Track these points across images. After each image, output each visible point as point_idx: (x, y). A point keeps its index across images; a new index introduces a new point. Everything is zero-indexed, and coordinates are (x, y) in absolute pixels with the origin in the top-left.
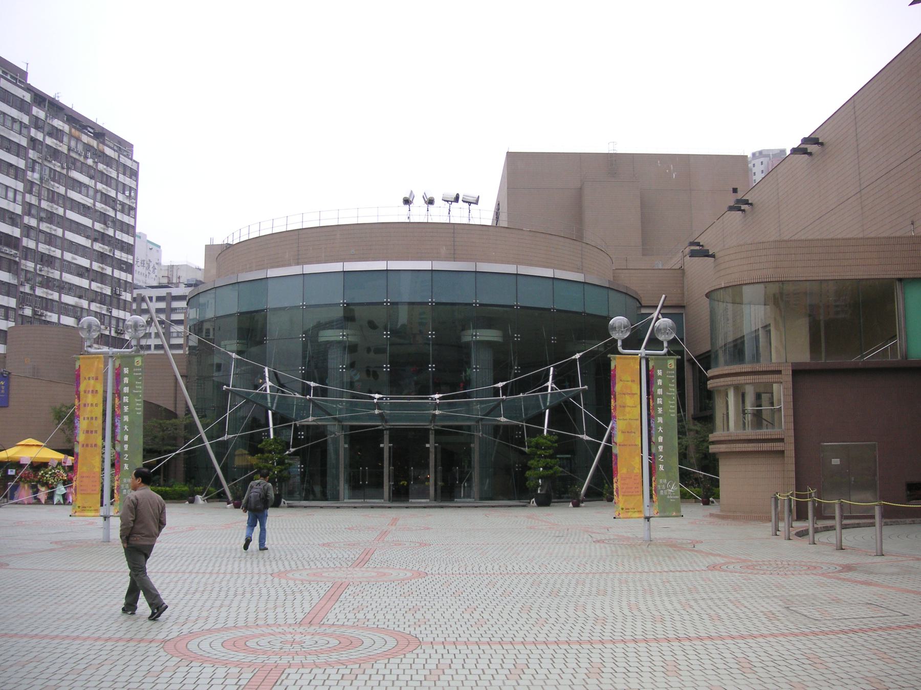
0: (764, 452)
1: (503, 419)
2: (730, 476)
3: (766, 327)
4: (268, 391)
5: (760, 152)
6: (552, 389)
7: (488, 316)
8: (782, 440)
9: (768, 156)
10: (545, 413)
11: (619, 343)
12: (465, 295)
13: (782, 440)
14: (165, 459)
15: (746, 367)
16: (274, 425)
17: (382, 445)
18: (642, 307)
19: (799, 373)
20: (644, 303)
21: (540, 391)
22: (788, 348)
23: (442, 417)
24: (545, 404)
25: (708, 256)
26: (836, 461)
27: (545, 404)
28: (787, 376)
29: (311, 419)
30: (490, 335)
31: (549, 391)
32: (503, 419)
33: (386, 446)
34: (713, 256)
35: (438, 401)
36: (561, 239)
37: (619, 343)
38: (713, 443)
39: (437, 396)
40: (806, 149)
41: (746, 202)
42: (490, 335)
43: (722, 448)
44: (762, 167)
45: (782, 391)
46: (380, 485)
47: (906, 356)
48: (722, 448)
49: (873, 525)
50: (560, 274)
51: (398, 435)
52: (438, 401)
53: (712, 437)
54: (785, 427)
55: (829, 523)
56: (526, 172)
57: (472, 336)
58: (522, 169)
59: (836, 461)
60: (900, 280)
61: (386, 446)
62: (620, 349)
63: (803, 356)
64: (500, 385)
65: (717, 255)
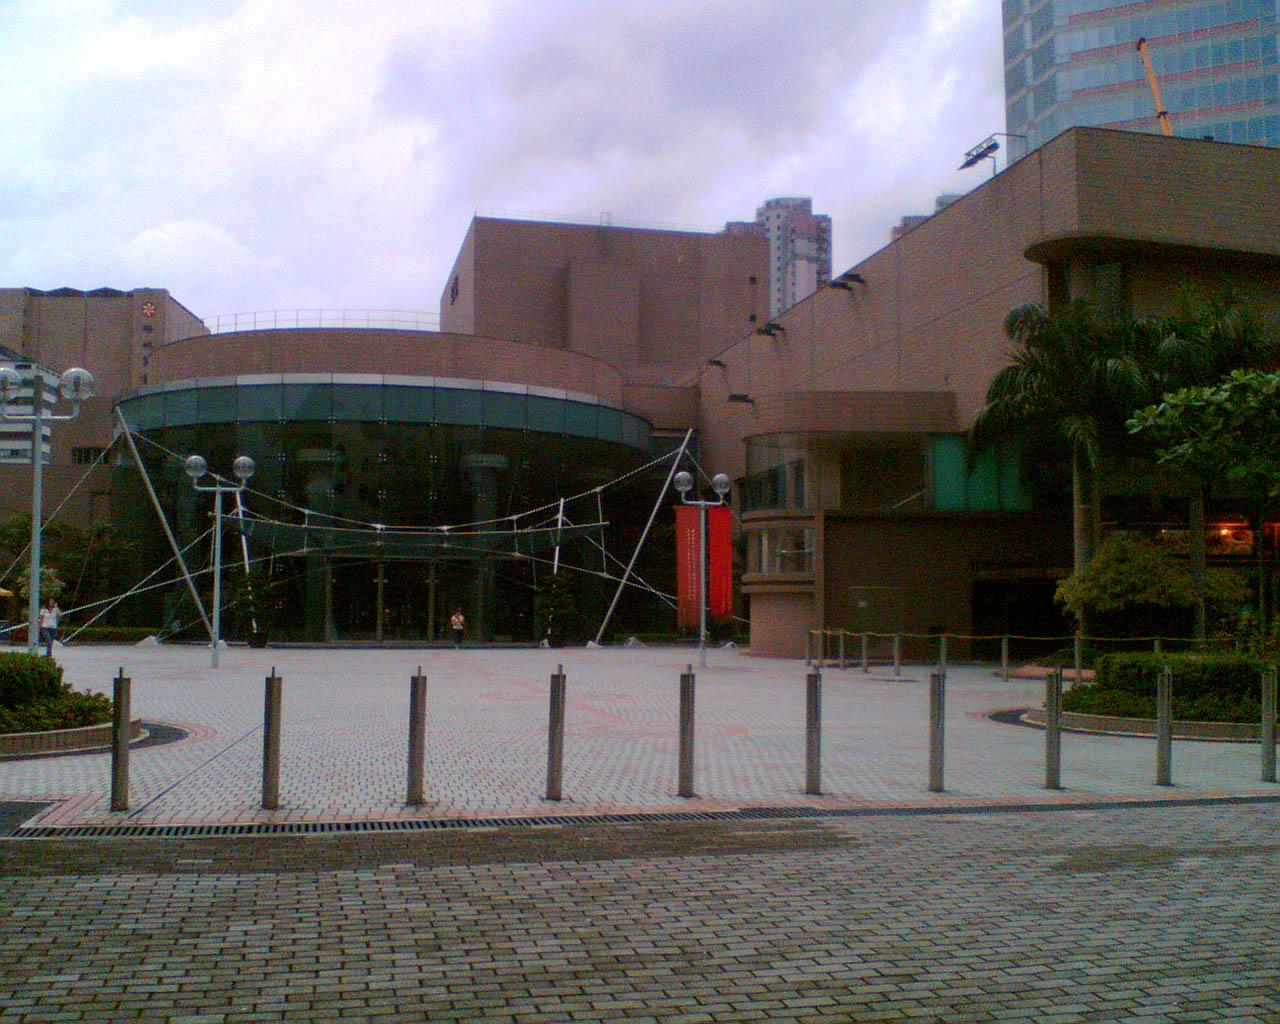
0: (793, 593)
1: (517, 554)
2: (761, 621)
3: (798, 467)
4: (241, 516)
6: (563, 525)
7: (493, 439)
8: (811, 583)
10: (555, 550)
11: (683, 495)
12: (471, 416)
13: (811, 583)
14: (139, 588)
15: (780, 512)
16: (249, 558)
17: (375, 581)
18: (654, 429)
19: (832, 521)
20: (656, 425)
21: (547, 526)
22: (822, 491)
23: (453, 551)
24: (555, 540)
25: (747, 401)
26: (862, 604)
27: (555, 540)
28: (819, 523)
29: (305, 550)
30: (497, 461)
32: (517, 554)
33: (381, 581)
34: (751, 401)
35: (447, 533)
36: (1195, 808)
37: (683, 495)
38: (745, 584)
39: (445, 528)
40: (846, 284)
41: (777, 327)
42: (497, 461)
43: (756, 589)
45: (814, 538)
46: (425, 629)
47: (931, 507)
48: (756, 589)
49: (893, 664)
50: (573, 396)
51: (393, 569)
52: (447, 533)
53: (745, 578)
54: (816, 569)
55: (836, 662)
56: (499, 252)
57: (477, 462)
58: (493, 243)
59: (862, 604)
60: (933, 435)
61: (381, 581)
62: (683, 500)
63: (836, 504)
64: (514, 517)
65: (756, 402)
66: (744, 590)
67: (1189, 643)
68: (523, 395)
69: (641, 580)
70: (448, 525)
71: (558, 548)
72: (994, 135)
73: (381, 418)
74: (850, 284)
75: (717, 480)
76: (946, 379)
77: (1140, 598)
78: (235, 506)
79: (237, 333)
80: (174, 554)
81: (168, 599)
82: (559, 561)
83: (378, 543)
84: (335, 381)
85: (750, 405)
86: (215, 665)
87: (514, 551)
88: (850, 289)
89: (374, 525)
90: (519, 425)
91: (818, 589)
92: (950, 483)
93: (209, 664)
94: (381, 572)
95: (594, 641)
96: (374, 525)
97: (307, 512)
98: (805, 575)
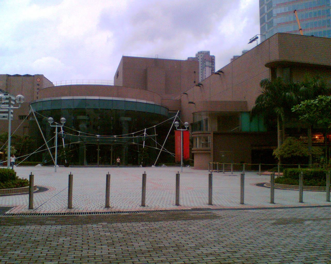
0: (205, 153)
1: (134, 143)
2: (197, 160)
3: (206, 120)
4: (62, 133)
5: (201, 52)
6: (146, 135)
7: (128, 113)
8: (210, 150)
9: (204, 53)
10: (143, 142)
11: (177, 128)
12: (122, 107)
13: (210, 150)
14: (36, 152)
15: (202, 132)
16: (65, 144)
17: (97, 150)
18: (169, 111)
19: (215, 134)
20: (170, 110)
21: (142, 135)
22: (213, 127)
23: (117, 142)
24: (144, 139)
25: (193, 103)
26: (223, 156)
27: (144, 139)
28: (212, 135)
29: (79, 142)
30: (129, 119)
31: (145, 136)
32: (134, 143)
33: (98, 150)
34: (194, 103)
35: (116, 138)
36: (309, 208)
37: (177, 128)
38: (193, 151)
39: (115, 136)
40: (219, 73)
41: (201, 84)
42: (129, 119)
43: (196, 152)
44: (201, 57)
45: (210, 139)
47: (241, 131)
48: (196, 152)
49: (231, 171)
50: (148, 102)
51: (102, 147)
52: (116, 138)
53: (193, 149)
54: (211, 147)
56: (129, 65)
57: (123, 119)
58: (127, 63)
59: (223, 156)
60: (241, 112)
61: (98, 150)
62: (177, 129)
63: (216, 130)
64: (133, 133)
65: (196, 104)
66: (193, 152)
67: (308, 166)
68: (135, 102)
69: (166, 150)
70: (116, 135)
71: (144, 141)
72: (257, 35)
73: (98, 108)
74: (220, 73)
75: (185, 124)
76: (245, 98)
77: (295, 154)
78: (61, 131)
79: (61, 86)
80: (45, 143)
81: (43, 154)
82: (145, 145)
83: (98, 140)
84: (87, 98)
85: (194, 104)
86: (56, 172)
87: (133, 142)
88: (220, 74)
89: (97, 135)
90: (134, 110)
91: (212, 152)
92: (246, 124)
93: (54, 171)
94: (98, 148)
95: (154, 165)
96: (97, 135)
97: (79, 132)
98: (208, 148)
